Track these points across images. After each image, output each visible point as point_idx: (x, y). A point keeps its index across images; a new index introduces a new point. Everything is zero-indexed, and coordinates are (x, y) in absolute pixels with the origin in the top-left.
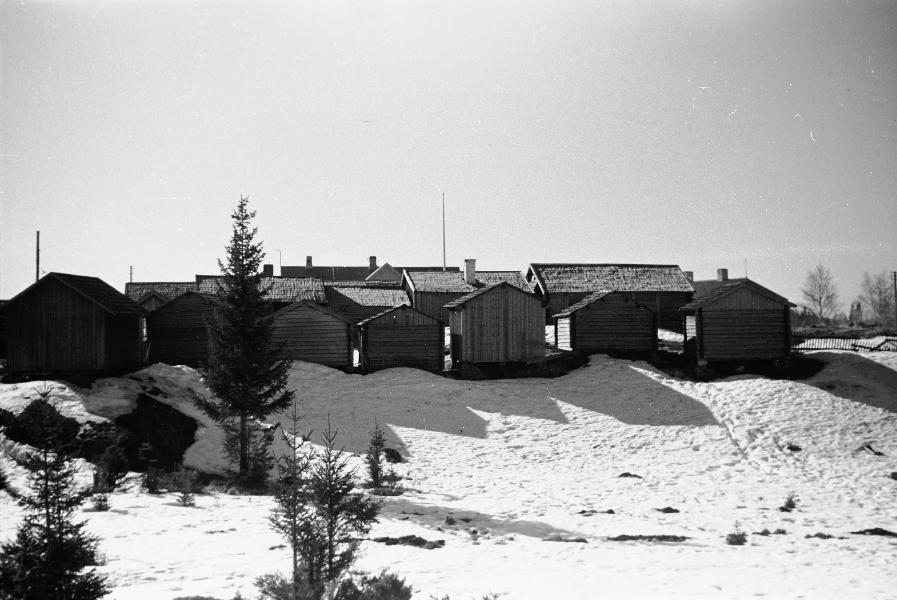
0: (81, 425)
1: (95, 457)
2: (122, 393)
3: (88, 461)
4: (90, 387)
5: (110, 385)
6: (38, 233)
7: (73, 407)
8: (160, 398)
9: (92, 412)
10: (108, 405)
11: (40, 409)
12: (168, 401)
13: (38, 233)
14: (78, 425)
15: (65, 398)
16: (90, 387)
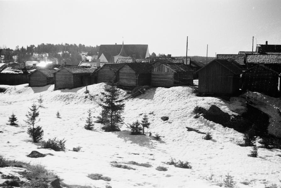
0: (230, 116)
1: (67, 45)
2: (241, 104)
3: (235, 130)
4: (229, 101)
5: (236, 100)
6: (187, 37)
7: (225, 109)
8: (253, 105)
9: (233, 111)
10: (238, 108)
11: (214, 108)
12: (256, 107)
13: (187, 37)
14: (229, 116)
15: (222, 105)
16: (229, 101)
